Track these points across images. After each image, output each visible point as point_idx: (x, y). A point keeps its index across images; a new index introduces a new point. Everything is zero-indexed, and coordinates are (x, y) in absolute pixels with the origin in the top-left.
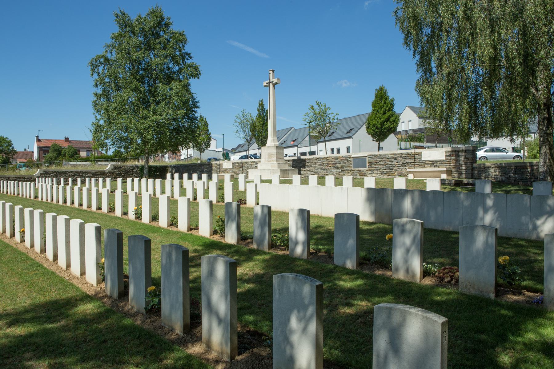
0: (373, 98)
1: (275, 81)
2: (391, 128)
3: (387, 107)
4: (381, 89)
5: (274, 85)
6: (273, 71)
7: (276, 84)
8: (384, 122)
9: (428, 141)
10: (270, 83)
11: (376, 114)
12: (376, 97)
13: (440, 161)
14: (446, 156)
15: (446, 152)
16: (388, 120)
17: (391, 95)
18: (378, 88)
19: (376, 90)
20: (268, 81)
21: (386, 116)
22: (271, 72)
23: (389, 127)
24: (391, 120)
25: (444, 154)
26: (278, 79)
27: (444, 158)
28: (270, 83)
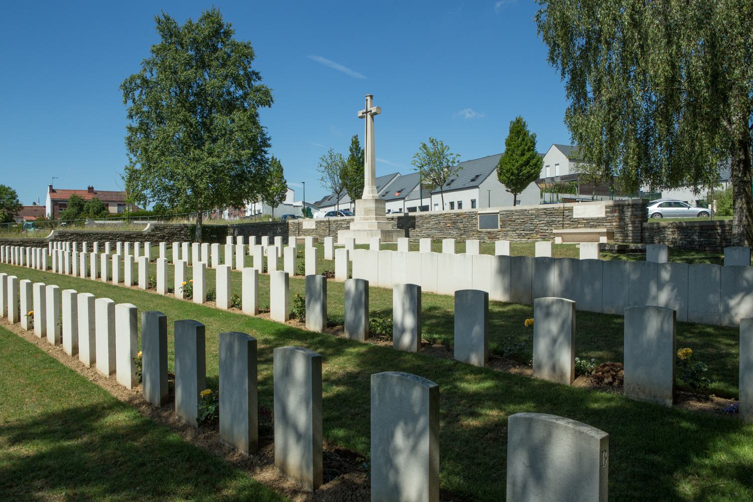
0: (506, 134)
1: (374, 110)
2: (532, 174)
3: (526, 145)
4: (518, 121)
5: (372, 116)
6: (371, 97)
7: (376, 114)
8: (522, 166)
9: (582, 192)
10: (367, 112)
11: (512, 155)
12: (511, 131)
13: (598, 219)
14: (606, 212)
15: (606, 207)
16: (527, 163)
17: (531, 129)
18: (514, 120)
19: (511, 122)
20: (365, 111)
21: (525, 158)
22: (369, 98)
23: (528, 172)
24: (531, 164)
25: (604, 210)
26: (378, 108)
27: (603, 215)
28: (367, 112)
